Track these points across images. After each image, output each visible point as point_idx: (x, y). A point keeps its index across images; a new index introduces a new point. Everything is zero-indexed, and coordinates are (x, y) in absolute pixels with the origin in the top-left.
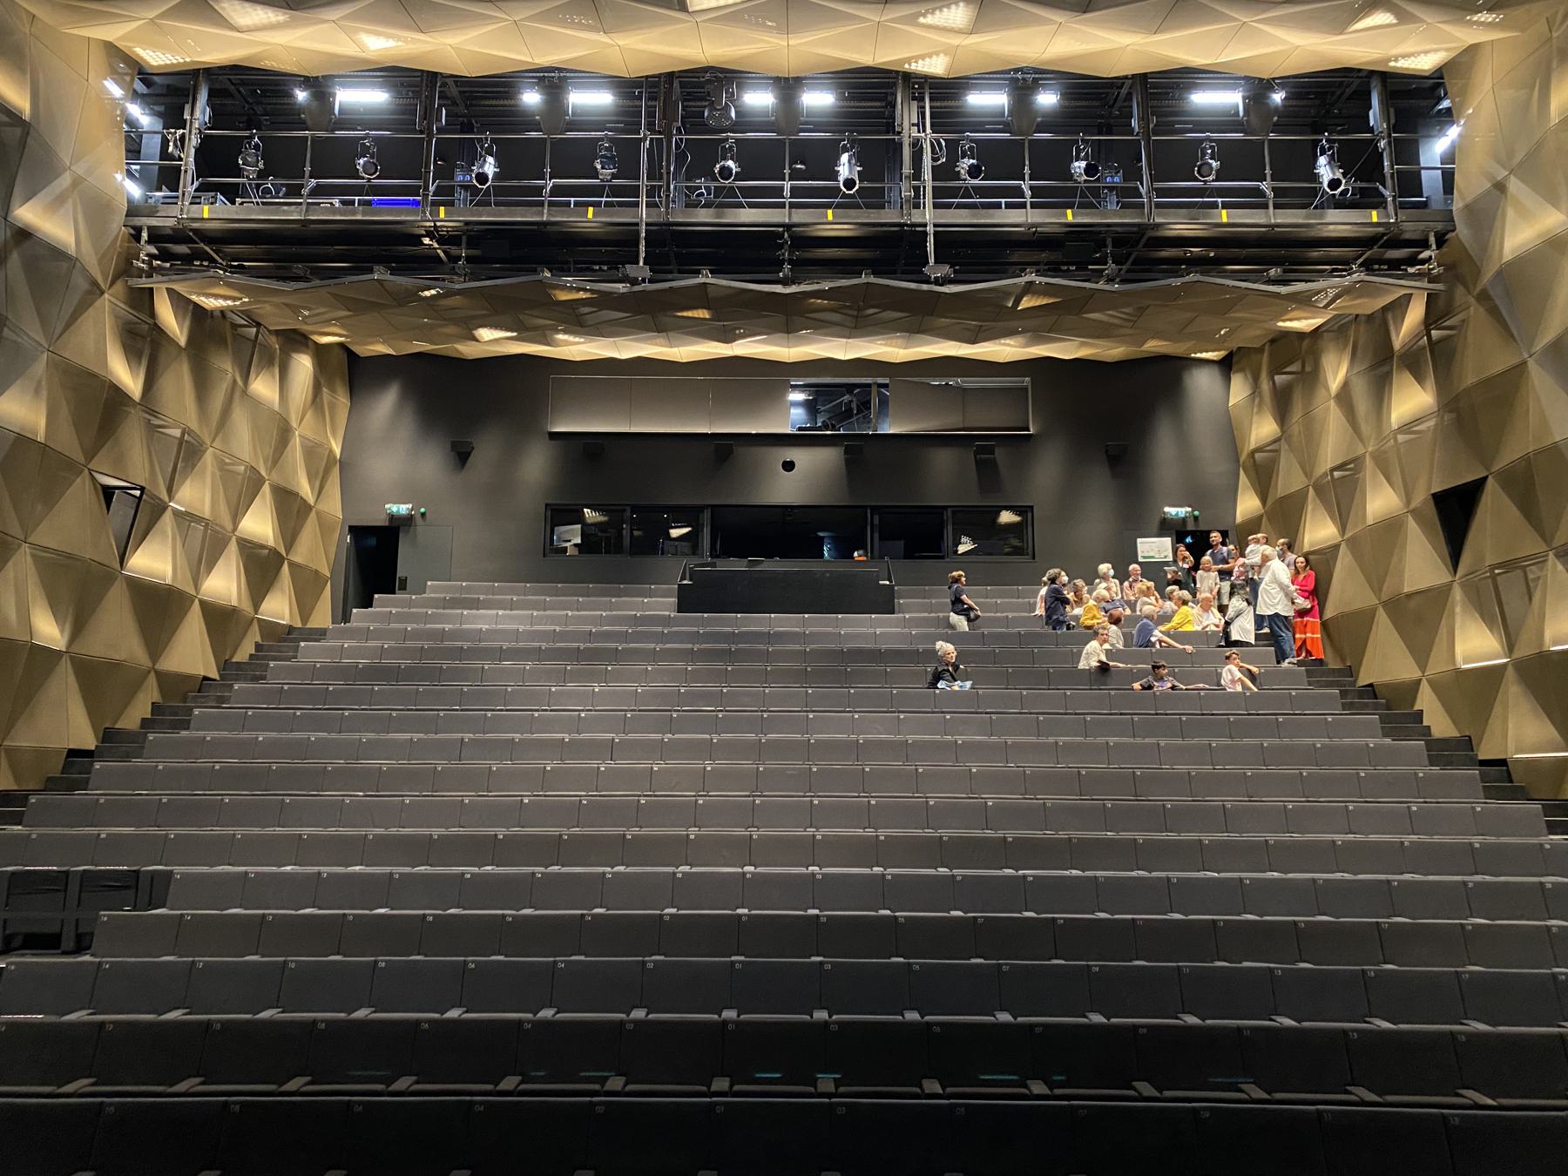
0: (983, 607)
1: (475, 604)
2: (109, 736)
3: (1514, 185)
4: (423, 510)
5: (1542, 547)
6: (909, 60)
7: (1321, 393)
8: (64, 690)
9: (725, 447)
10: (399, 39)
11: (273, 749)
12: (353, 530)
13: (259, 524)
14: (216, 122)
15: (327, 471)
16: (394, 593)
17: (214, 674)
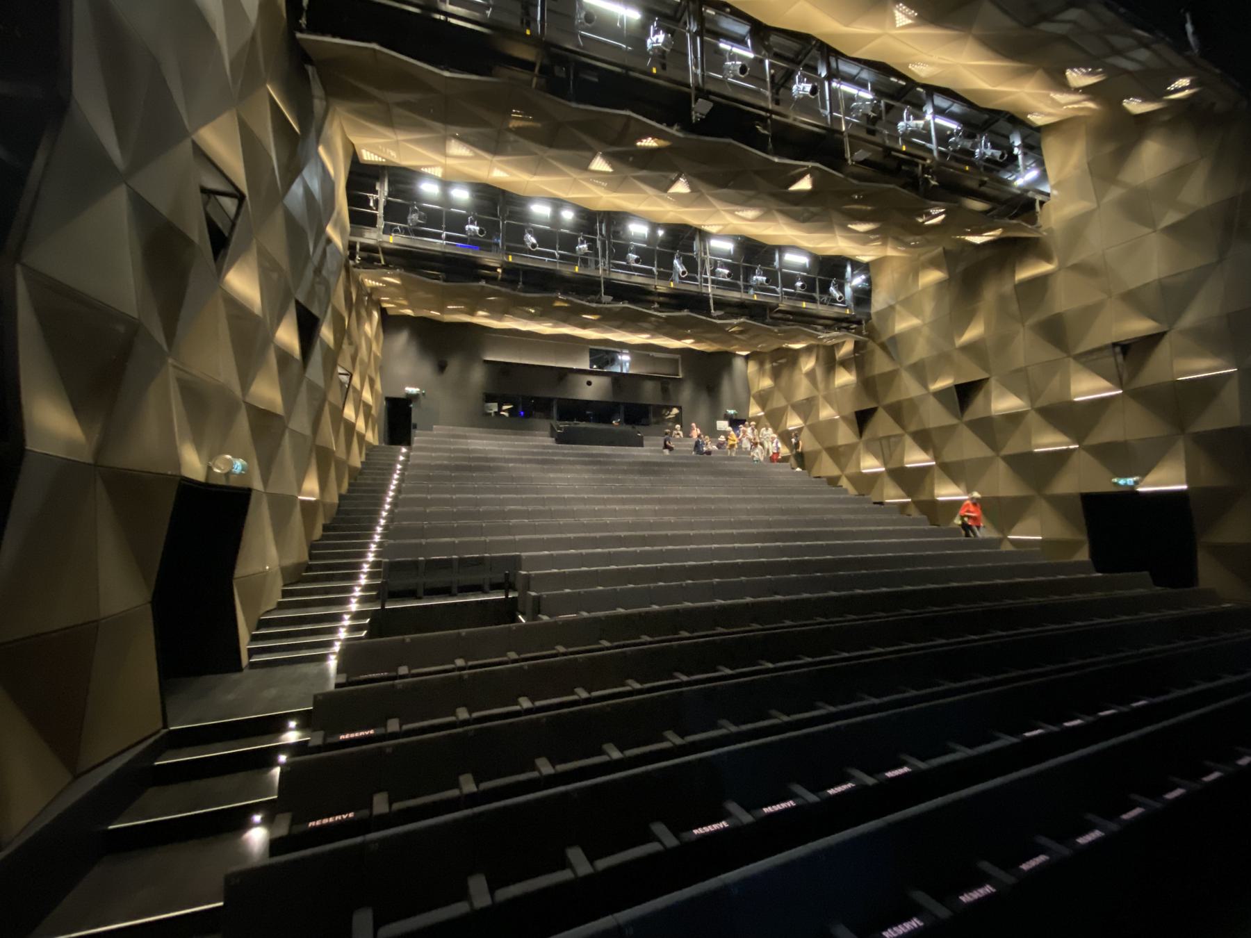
0: (677, 446)
1: (465, 437)
3: (898, 307)
5: (898, 431)
6: (704, 226)
7: (797, 372)
9: (564, 373)
10: (508, 173)
14: (390, 195)
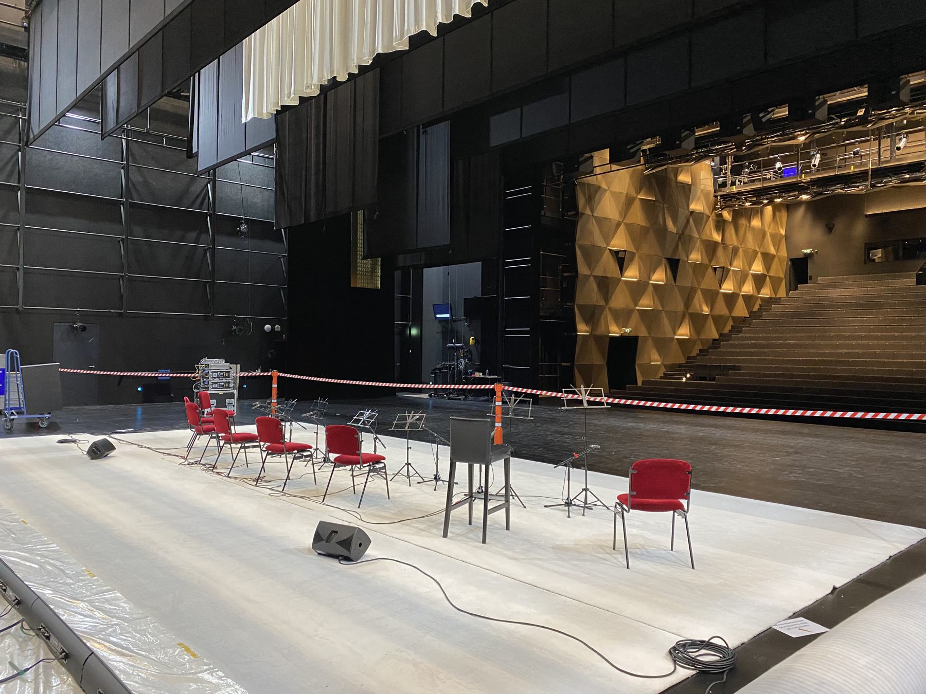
2: (721, 335)
4: (816, 250)
8: (710, 324)
11: (764, 338)
12: (791, 260)
13: (757, 267)
15: (780, 241)
16: (807, 283)
17: (748, 316)
